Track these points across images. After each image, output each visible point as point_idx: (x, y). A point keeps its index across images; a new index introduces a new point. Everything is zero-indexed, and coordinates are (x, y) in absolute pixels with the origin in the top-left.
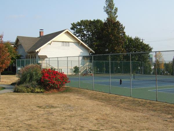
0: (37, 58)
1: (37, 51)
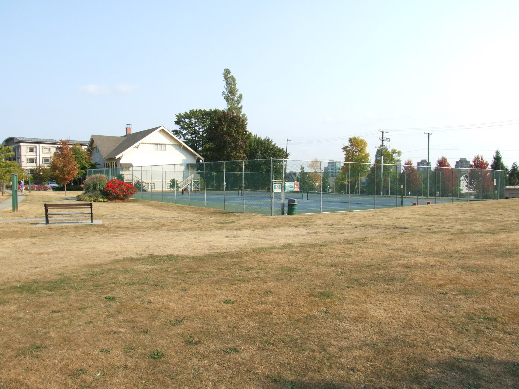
0: (119, 166)
1: (117, 157)
